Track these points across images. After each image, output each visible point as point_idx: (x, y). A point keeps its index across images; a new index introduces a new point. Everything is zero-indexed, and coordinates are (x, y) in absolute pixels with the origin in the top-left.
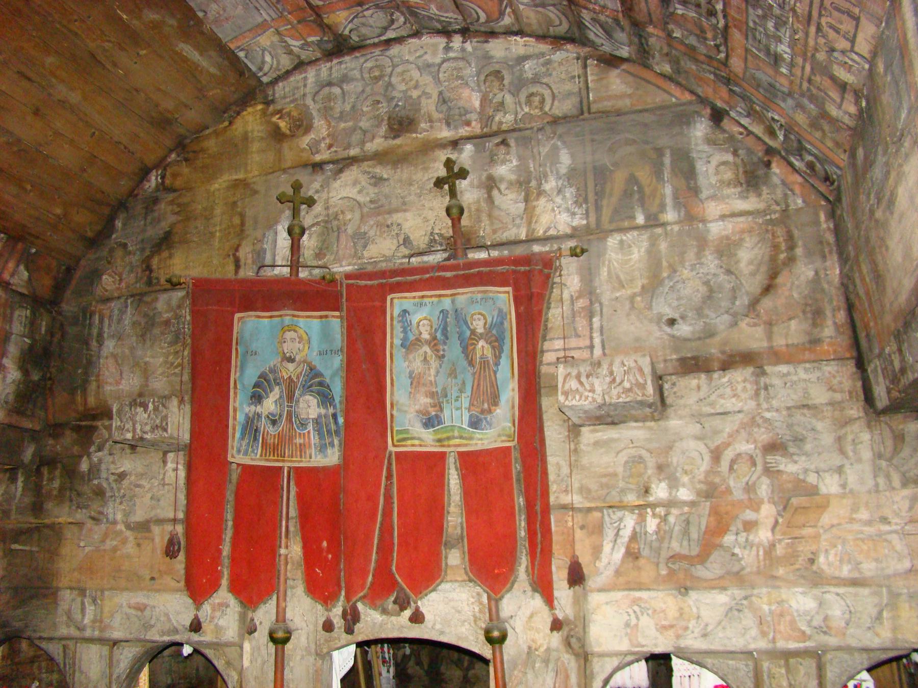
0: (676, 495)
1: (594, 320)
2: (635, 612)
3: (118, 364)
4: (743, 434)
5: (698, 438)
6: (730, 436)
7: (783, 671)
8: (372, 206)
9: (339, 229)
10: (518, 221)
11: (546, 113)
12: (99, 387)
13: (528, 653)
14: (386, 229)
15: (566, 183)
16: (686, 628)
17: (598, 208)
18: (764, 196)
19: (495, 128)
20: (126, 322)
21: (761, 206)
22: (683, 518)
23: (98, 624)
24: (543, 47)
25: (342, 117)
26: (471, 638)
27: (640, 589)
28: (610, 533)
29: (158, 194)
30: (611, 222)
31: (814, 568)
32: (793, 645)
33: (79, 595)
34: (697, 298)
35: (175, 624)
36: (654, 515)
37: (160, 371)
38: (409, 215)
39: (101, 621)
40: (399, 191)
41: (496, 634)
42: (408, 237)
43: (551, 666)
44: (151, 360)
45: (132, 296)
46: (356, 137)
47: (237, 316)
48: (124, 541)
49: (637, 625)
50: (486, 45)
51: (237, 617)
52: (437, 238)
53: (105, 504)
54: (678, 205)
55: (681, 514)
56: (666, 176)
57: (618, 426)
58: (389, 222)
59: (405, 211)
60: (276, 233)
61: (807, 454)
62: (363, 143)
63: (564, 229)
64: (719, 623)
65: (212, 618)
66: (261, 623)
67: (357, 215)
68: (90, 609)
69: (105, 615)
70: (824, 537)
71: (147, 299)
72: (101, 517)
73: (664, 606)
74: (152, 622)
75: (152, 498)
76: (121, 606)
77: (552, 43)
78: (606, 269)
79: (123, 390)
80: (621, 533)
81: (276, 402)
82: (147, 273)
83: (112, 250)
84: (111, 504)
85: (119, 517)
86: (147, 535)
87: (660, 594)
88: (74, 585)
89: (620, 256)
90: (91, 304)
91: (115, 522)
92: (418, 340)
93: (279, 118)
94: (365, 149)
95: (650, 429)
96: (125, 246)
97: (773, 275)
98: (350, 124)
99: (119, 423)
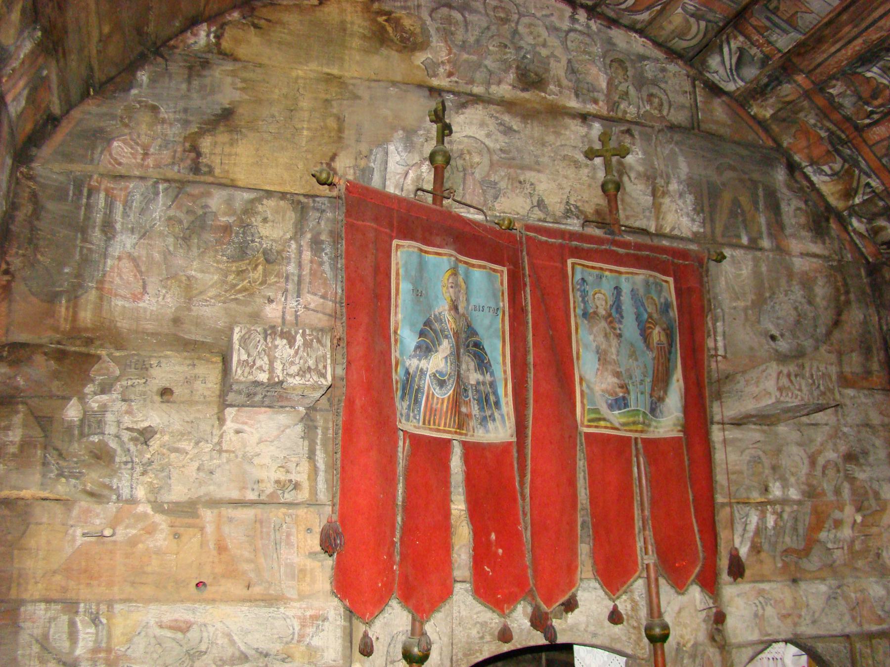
0: (788, 495)
1: (718, 324)
2: (760, 603)
3: (141, 272)
4: (830, 445)
5: (800, 444)
6: (822, 445)
7: (869, 651)
8: (503, 156)
9: (464, 170)
10: (647, 214)
11: (664, 117)
12: (101, 298)
13: (677, 649)
14: (518, 185)
15: (686, 189)
16: (800, 616)
17: (712, 220)
18: (827, 245)
19: (620, 115)
20: (156, 215)
21: (826, 253)
22: (793, 515)
23: (102, 655)
24: (659, 54)
25: (464, 46)
26: (624, 638)
27: (762, 581)
28: (739, 528)
29: (210, 56)
30: (723, 236)
31: (880, 562)
32: (874, 628)
33: (64, 611)
34: (791, 320)
35: (243, 648)
36: (774, 513)
37: (212, 292)
38: (542, 177)
39: (109, 650)
40: (532, 148)
41: (657, 631)
42: (543, 201)
43: (698, 661)
44: (199, 275)
45: (167, 180)
46: (479, 76)
47: (395, 242)
48: (151, 530)
49: (763, 615)
50: (609, 30)
51: (339, 632)
52: (573, 209)
53: (114, 473)
54: (770, 235)
55: (792, 512)
56: (761, 206)
57: (742, 427)
58: (522, 179)
59: (539, 171)
60: (387, 153)
61: (871, 466)
62: (489, 84)
63: (686, 233)
64: (823, 610)
65: (302, 637)
66: (378, 638)
67: (486, 161)
68: (87, 635)
69: (115, 641)
70: (884, 535)
71: (189, 189)
72: (106, 492)
73: (782, 596)
74: (203, 647)
75: (198, 469)
76: (147, 626)
77: (666, 53)
78: (723, 278)
79: (145, 309)
80: (747, 528)
81: (446, 358)
82: (193, 155)
83: (129, 109)
84: (126, 475)
85: (141, 493)
86: (191, 521)
87: (779, 585)
88: (55, 595)
89: (733, 270)
90: (91, 177)
91: (133, 501)
92: (595, 313)
93: (386, 21)
94: (491, 90)
95: (764, 432)
96: (155, 109)
97: (839, 313)
98: (475, 58)
99: (244, 357)
